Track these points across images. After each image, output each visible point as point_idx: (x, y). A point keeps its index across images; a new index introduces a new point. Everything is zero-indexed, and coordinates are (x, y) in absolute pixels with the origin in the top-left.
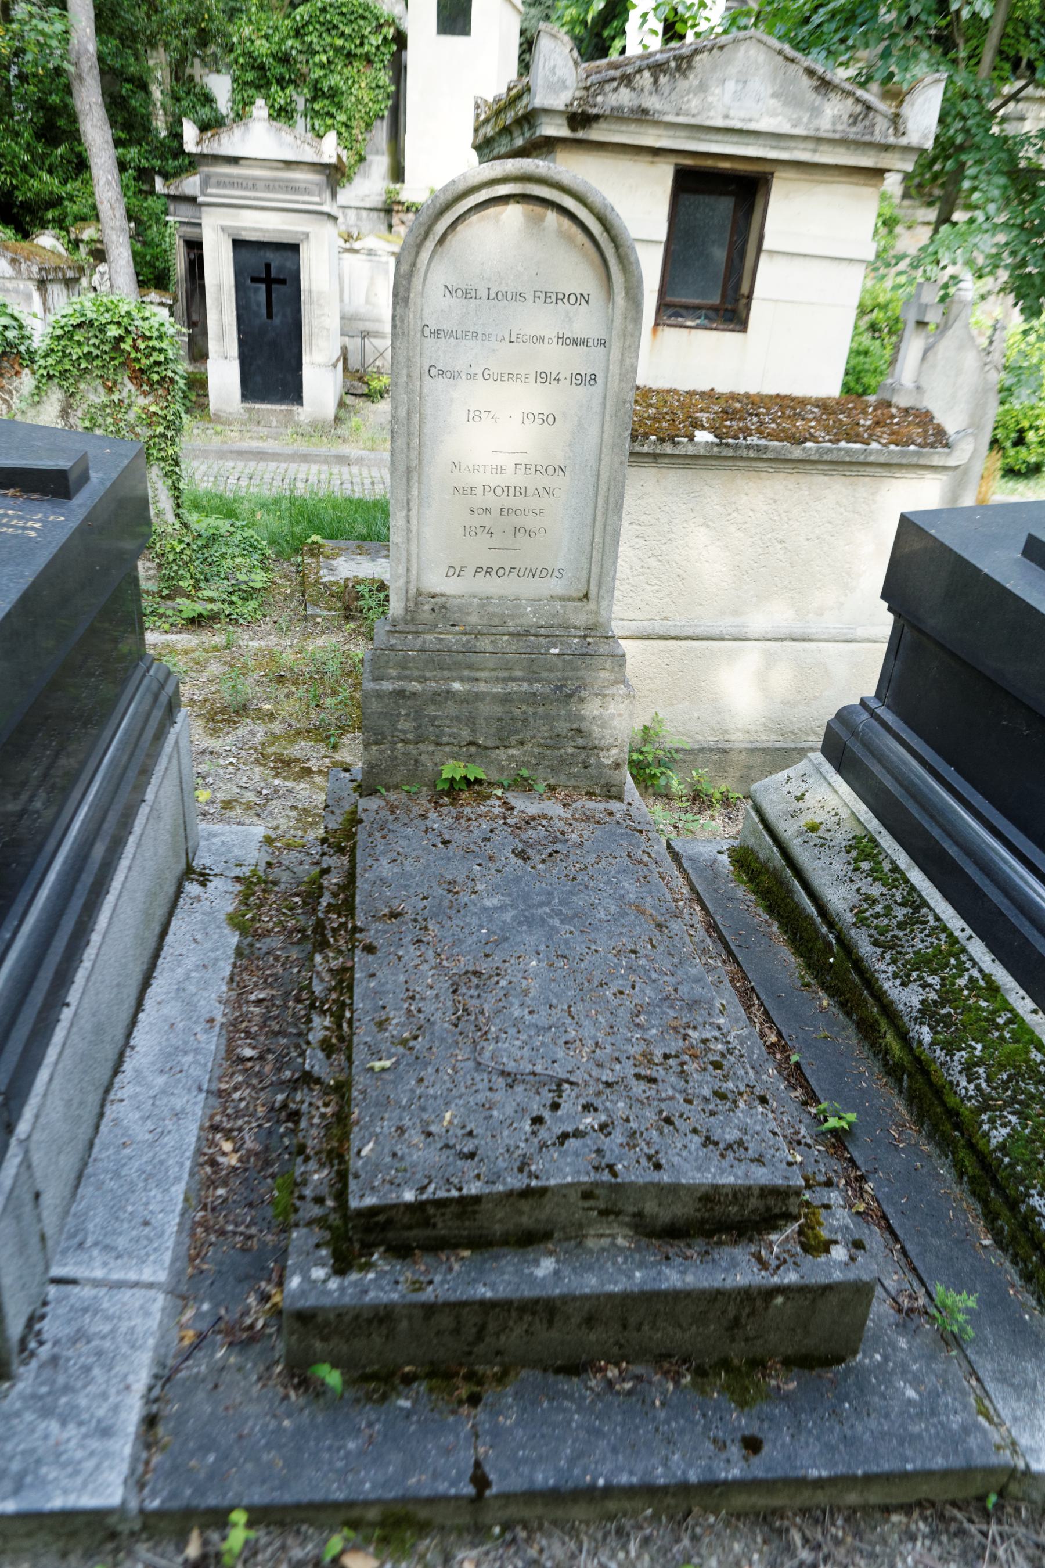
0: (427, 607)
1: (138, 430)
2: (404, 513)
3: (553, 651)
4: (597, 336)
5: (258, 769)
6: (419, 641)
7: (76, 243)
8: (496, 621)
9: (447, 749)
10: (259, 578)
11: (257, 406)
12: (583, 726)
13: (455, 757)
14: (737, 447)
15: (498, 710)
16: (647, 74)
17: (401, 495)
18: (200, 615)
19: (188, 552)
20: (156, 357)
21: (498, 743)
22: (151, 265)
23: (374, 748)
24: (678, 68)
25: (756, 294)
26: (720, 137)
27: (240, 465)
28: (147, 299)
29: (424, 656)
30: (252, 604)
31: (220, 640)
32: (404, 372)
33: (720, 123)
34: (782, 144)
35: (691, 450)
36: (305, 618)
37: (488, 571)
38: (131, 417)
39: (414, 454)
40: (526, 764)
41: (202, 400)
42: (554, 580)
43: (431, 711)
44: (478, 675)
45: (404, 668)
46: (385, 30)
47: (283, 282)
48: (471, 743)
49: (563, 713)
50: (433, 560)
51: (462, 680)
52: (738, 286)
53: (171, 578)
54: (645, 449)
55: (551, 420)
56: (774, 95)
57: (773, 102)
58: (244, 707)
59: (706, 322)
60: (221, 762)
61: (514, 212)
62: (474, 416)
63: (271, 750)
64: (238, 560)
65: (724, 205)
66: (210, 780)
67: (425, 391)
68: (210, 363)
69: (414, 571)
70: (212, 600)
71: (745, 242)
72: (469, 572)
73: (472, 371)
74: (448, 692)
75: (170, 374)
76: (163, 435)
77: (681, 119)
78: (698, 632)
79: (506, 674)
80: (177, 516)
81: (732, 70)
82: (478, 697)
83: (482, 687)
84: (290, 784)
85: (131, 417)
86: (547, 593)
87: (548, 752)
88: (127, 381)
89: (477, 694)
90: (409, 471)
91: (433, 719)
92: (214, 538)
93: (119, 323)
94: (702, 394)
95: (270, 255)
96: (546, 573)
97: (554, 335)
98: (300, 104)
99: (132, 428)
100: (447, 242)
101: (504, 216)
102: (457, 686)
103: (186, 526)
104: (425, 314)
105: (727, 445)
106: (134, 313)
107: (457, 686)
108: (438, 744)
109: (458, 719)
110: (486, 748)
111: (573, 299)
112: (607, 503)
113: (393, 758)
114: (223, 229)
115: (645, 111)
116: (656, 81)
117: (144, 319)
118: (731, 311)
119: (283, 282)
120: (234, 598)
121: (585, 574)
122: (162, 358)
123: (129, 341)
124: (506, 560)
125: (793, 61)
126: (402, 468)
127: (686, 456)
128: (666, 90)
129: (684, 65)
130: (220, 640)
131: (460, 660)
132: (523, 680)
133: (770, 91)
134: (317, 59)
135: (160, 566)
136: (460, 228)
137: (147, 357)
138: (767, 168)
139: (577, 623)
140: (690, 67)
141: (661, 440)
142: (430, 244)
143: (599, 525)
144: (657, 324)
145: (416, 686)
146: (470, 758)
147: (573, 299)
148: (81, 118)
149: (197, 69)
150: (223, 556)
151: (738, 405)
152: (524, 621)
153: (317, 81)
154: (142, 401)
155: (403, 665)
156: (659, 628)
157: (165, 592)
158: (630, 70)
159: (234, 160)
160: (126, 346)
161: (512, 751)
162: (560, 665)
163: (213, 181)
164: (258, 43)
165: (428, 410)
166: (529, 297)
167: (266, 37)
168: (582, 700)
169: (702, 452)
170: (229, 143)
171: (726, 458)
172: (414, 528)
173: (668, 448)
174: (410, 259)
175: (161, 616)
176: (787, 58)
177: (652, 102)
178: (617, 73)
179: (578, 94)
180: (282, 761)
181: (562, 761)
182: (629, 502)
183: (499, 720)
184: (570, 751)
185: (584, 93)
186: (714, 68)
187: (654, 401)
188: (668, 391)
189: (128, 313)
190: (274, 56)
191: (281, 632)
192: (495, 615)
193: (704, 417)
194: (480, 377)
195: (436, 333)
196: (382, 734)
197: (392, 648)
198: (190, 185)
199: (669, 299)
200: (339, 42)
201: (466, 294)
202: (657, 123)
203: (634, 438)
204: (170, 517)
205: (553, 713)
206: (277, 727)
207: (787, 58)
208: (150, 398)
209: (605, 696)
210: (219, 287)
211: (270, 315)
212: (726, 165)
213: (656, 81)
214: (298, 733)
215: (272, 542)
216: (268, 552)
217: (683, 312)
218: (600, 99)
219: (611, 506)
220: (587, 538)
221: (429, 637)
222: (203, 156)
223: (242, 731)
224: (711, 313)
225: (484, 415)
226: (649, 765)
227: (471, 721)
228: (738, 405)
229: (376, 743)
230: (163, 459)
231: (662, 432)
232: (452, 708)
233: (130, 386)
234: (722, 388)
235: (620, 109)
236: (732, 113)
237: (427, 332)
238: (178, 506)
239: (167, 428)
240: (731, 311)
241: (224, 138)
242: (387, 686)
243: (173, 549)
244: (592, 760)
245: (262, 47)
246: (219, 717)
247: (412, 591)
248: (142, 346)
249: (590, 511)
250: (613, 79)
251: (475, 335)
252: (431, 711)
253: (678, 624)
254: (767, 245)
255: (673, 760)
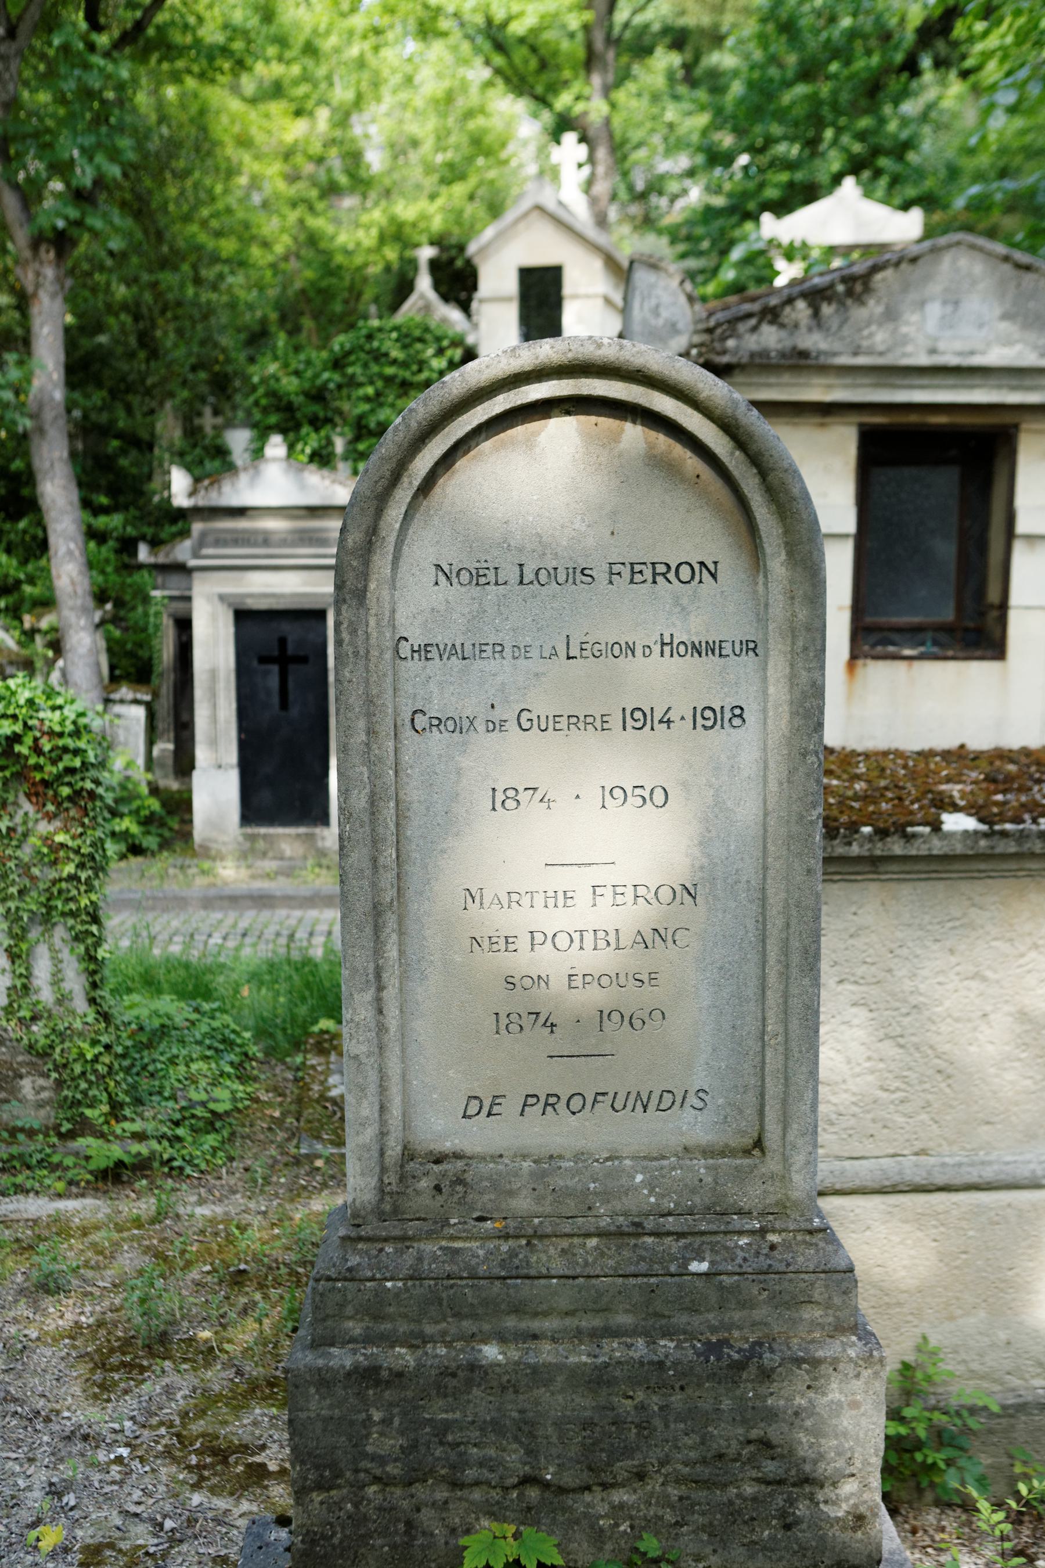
0: (424, 1184)
1: (36, 871)
2: (369, 995)
3: (695, 1267)
4: (738, 635)
5: (166, 1471)
6: (409, 1258)
7: (30, 634)
8: (571, 1206)
9: (477, 1495)
10: (223, 1099)
11: (263, 830)
12: (774, 1433)
13: (495, 1512)
14: (1022, 836)
15: (584, 1403)
16: (801, 305)
17: (363, 959)
18: (120, 1164)
19: (106, 1059)
20: (68, 761)
21: (586, 1477)
22: (131, 654)
23: (317, 1497)
24: (850, 293)
25: (1016, 597)
26: (925, 381)
27: (232, 916)
28: (116, 696)
29: (419, 1290)
30: (211, 1140)
31: (146, 1206)
32: (362, 724)
33: (923, 360)
34: (1028, 382)
35: (938, 846)
36: (297, 1161)
37: (550, 1102)
38: (25, 854)
39: (387, 878)
40: (653, 1525)
41: (186, 828)
42: (689, 1114)
43: (438, 1411)
44: (535, 1325)
45: (377, 1318)
46: (449, 353)
47: (303, 660)
48: (527, 1480)
49: (726, 1404)
50: (429, 1085)
51: (502, 1338)
52: (981, 592)
53: (76, 1103)
54: (855, 850)
55: (659, 797)
56: (1005, 317)
57: (1004, 326)
58: (163, 1338)
59: (935, 650)
60: (102, 1456)
61: (562, 433)
62: (505, 799)
63: (198, 1427)
64: (194, 1067)
65: (943, 483)
66: (70, 1499)
67: (406, 758)
68: (197, 776)
69: (396, 1111)
70: (140, 1137)
71: (985, 527)
72: (511, 1106)
73: (497, 715)
74: (473, 1367)
75: (89, 785)
76: (73, 878)
77: (861, 360)
78: (988, 1174)
79: (597, 1322)
80: (92, 1001)
81: (935, 288)
82: (540, 1375)
83: (546, 1353)
84: (221, 1503)
85: (25, 854)
86: (674, 1142)
87: (702, 1494)
88: (23, 800)
89: (535, 1369)
90: (377, 911)
91: (442, 1429)
92: (164, 1031)
93: (15, 717)
94: (946, 755)
95: (286, 628)
96: (670, 1100)
97: (653, 639)
98: (339, 445)
99: (25, 869)
100: (437, 490)
101: (543, 439)
102: (491, 1352)
103: (105, 1017)
104: (401, 618)
105: (1004, 834)
106: (40, 700)
107: (491, 1352)
108: (456, 1485)
109: (497, 1427)
110: (562, 1490)
111: (685, 573)
112: (785, 950)
113: (358, 1520)
114: (222, 598)
115: (804, 354)
116: (816, 313)
117: (54, 708)
118: (977, 631)
119: (303, 660)
120: (180, 1132)
121: (751, 1098)
122: (77, 763)
123: (28, 740)
124: (588, 1077)
125: (1028, 268)
126: (362, 905)
127: (930, 858)
128: (834, 324)
129: (858, 287)
130: (146, 1206)
131: (499, 1296)
132: (634, 1333)
133: (998, 311)
134: (361, 392)
135: (59, 1084)
136: (461, 464)
137: (54, 762)
138: (1007, 419)
139: (744, 1203)
140: (867, 289)
141: (882, 833)
142: (403, 495)
143: (773, 998)
144: (854, 656)
145: (404, 1357)
146: (528, 1515)
147: (685, 573)
148: (39, 477)
149: (208, 421)
150: (173, 1061)
151: (1012, 768)
152: (629, 1203)
153: (361, 417)
154: (44, 827)
155: (375, 1309)
156: (912, 1169)
157: (66, 1127)
158: (774, 301)
159: (241, 512)
160: (22, 749)
161: (620, 1496)
162: (713, 1298)
163: (210, 539)
164: (285, 381)
165: (414, 793)
166: (601, 576)
167: (297, 373)
168: (766, 1375)
169: (959, 848)
170: (239, 492)
171: (1005, 857)
172: (393, 1024)
173: (897, 847)
174: (367, 521)
175: (54, 1168)
176: (1019, 266)
177: (813, 341)
178: (756, 307)
179: (697, 339)
180: (215, 1452)
181: (732, 1513)
182: (831, 945)
183: (587, 1424)
184: (749, 1489)
185: (705, 337)
186: (906, 288)
187: (862, 769)
188: (885, 754)
189: (31, 702)
190: (307, 394)
191: (254, 1186)
192: (569, 1193)
193: (955, 790)
194: (512, 726)
195: (423, 651)
196: (333, 1465)
197: (351, 1275)
198: (183, 551)
199: (869, 620)
200: (390, 371)
201: (477, 577)
202: (824, 369)
203: (831, 832)
204: (80, 1004)
205: (706, 1405)
206: (217, 1377)
207: (1019, 266)
208: (58, 823)
209: (816, 1362)
210: (213, 673)
211: (284, 704)
212: (941, 419)
213: (816, 313)
214: (253, 1387)
215: (262, 1032)
216: (254, 1050)
217: (895, 637)
218: (731, 343)
219: (795, 959)
220: (752, 1026)
221: (430, 1247)
222: (198, 512)
223: (151, 1387)
224: (942, 637)
225: (524, 797)
226: (919, 1445)
227: (525, 1430)
228: (1012, 768)
229: (320, 1487)
230: (73, 914)
231: (873, 825)
232: (480, 1403)
233: (27, 807)
234: (980, 741)
235: (764, 353)
236: (941, 346)
237: (405, 649)
238: (94, 985)
239: (81, 866)
240: (977, 631)
241: (227, 487)
242: (341, 1358)
243: (82, 1055)
244: (802, 1509)
245: (290, 384)
246: (114, 1360)
247: (394, 1151)
248: (47, 747)
249: (751, 969)
250: (749, 316)
251: (499, 648)
252: (438, 1411)
253: (948, 1159)
254: (1022, 526)
255: (967, 1431)
